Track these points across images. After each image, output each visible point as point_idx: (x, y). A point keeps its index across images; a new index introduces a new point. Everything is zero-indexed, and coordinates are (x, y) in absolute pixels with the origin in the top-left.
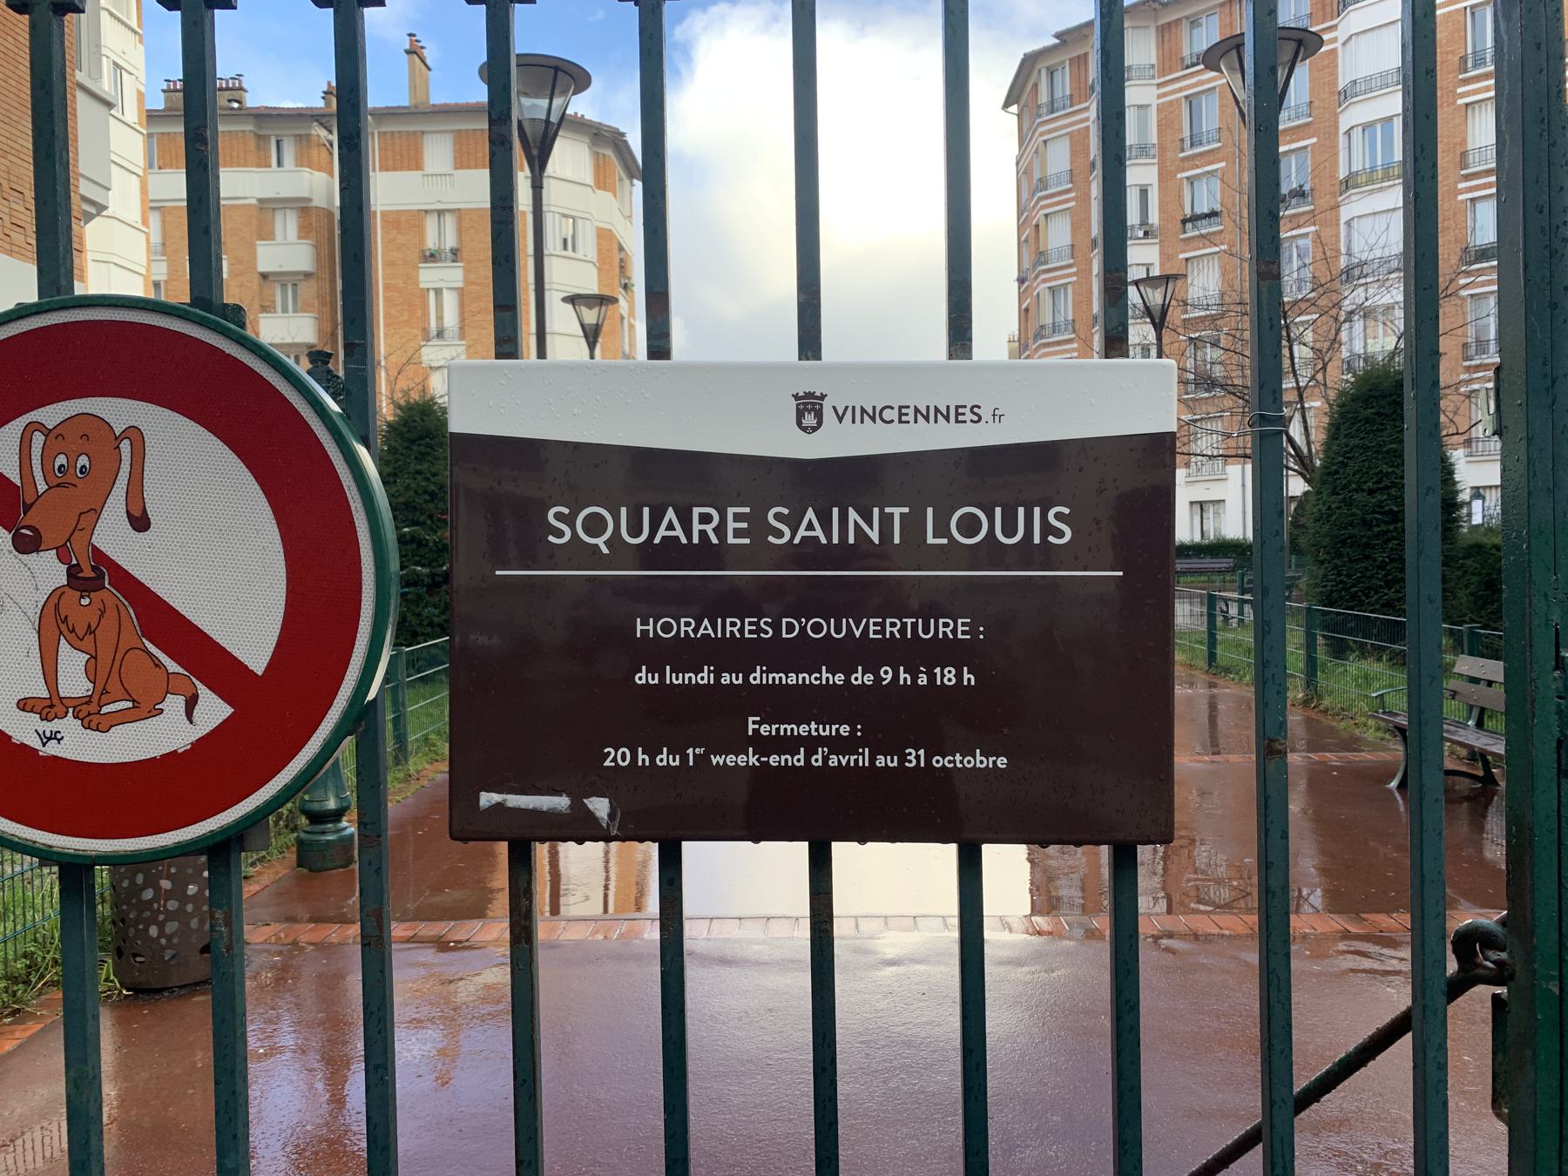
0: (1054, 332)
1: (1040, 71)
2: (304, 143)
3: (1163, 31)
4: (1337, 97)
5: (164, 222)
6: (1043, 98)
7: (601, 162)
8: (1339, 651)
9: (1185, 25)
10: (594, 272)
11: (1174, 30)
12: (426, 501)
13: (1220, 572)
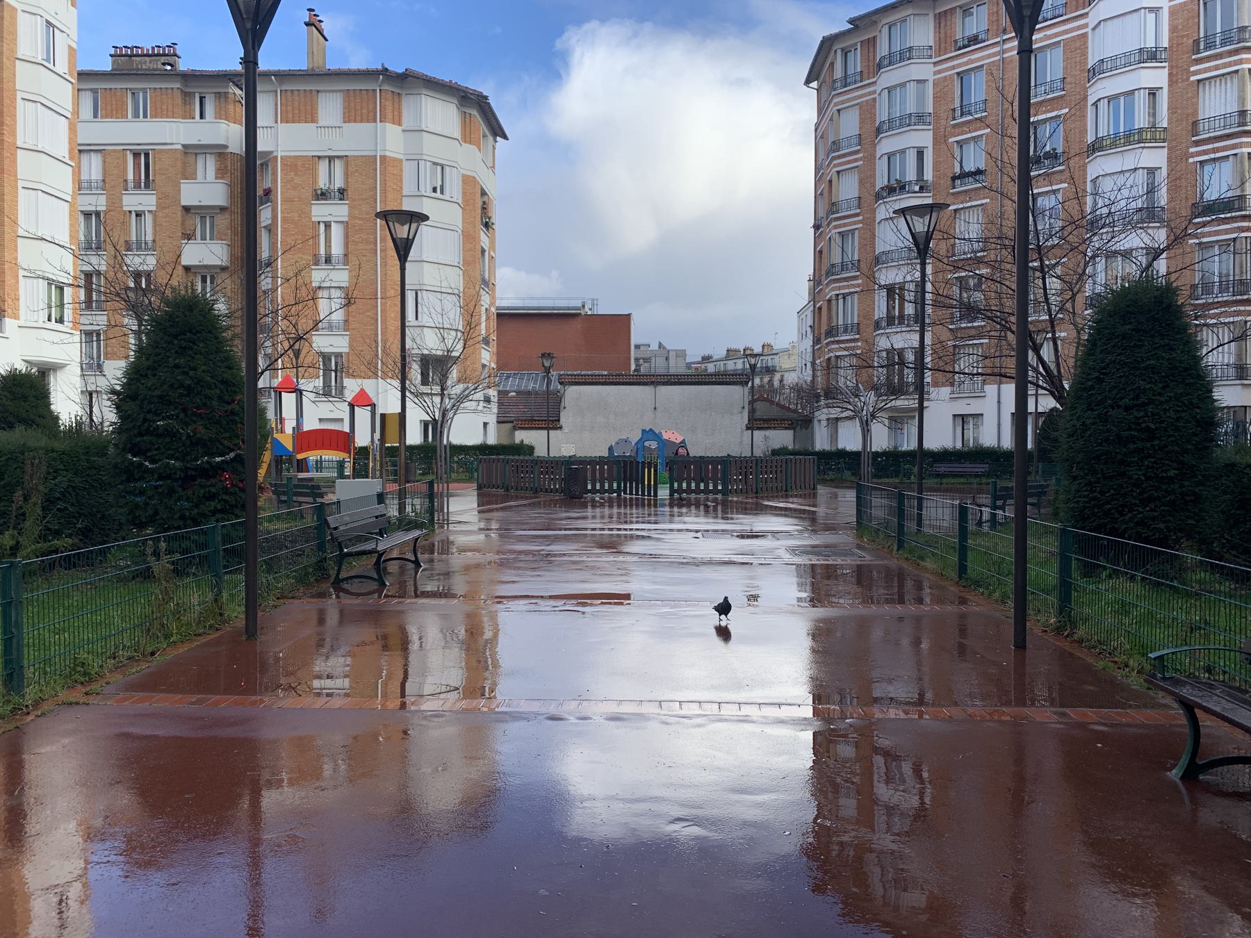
0: (842, 270)
1: (836, 51)
2: (222, 100)
3: (941, 18)
4: (1086, 74)
5: (104, 162)
6: (838, 73)
7: (468, 120)
8: (1090, 571)
9: (959, 12)
10: (460, 211)
11: (949, 18)
12: (182, 395)
13: (977, 476)
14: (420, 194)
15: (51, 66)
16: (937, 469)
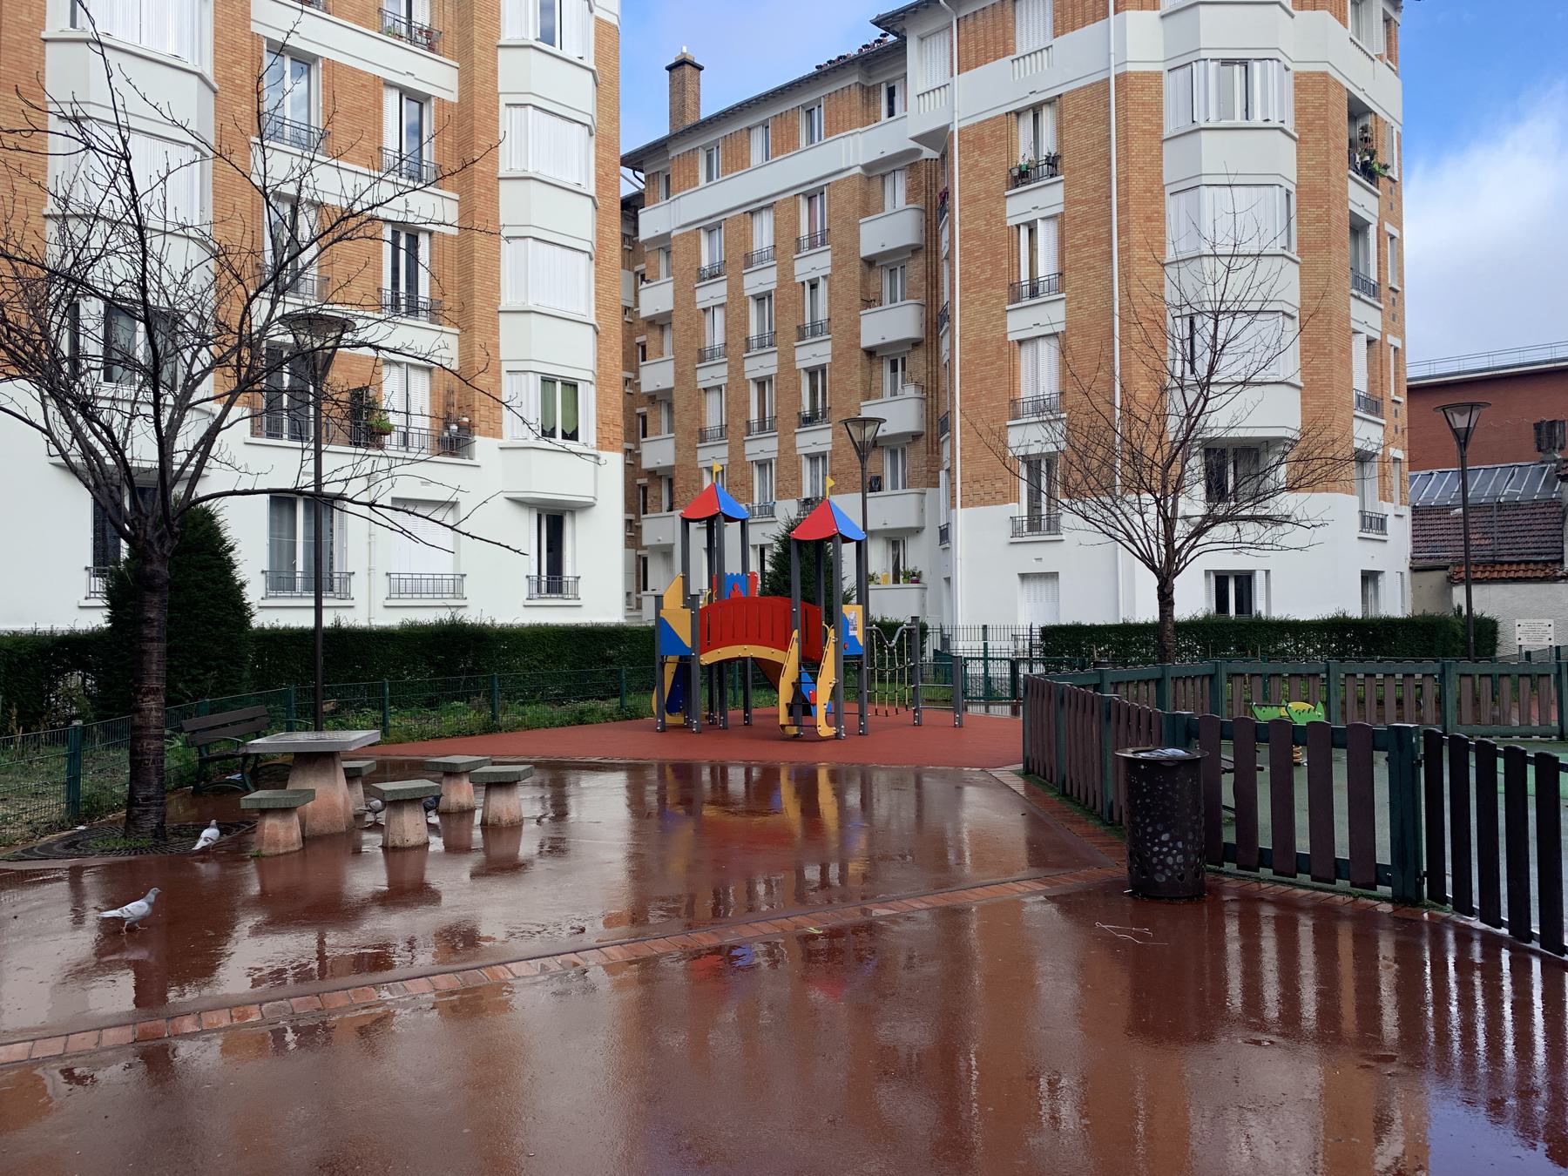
14: (1195, 127)
15: (556, 50)
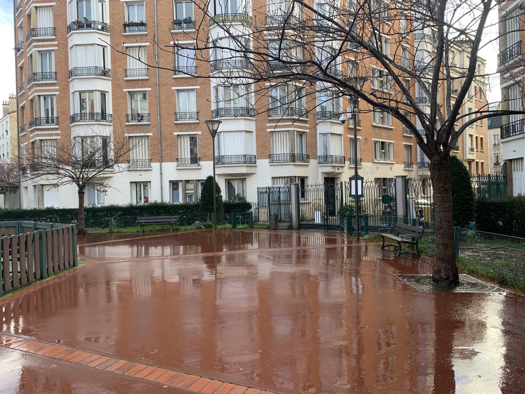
16: (140, 221)
